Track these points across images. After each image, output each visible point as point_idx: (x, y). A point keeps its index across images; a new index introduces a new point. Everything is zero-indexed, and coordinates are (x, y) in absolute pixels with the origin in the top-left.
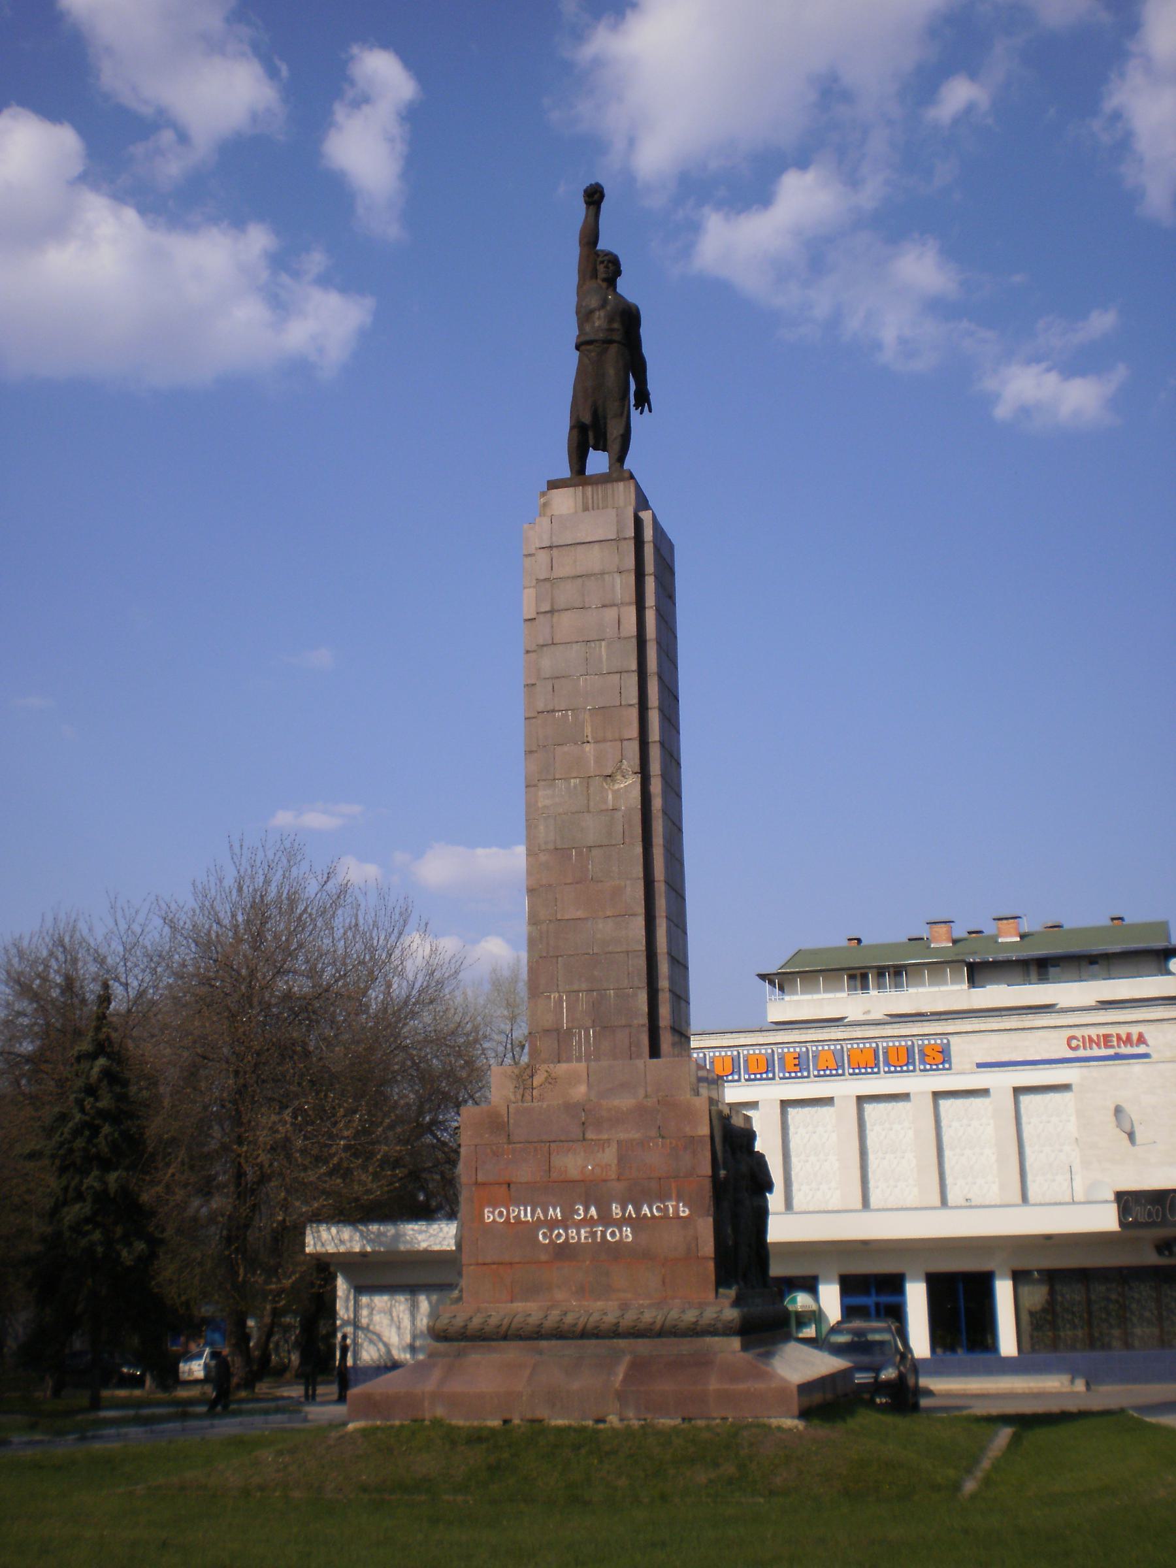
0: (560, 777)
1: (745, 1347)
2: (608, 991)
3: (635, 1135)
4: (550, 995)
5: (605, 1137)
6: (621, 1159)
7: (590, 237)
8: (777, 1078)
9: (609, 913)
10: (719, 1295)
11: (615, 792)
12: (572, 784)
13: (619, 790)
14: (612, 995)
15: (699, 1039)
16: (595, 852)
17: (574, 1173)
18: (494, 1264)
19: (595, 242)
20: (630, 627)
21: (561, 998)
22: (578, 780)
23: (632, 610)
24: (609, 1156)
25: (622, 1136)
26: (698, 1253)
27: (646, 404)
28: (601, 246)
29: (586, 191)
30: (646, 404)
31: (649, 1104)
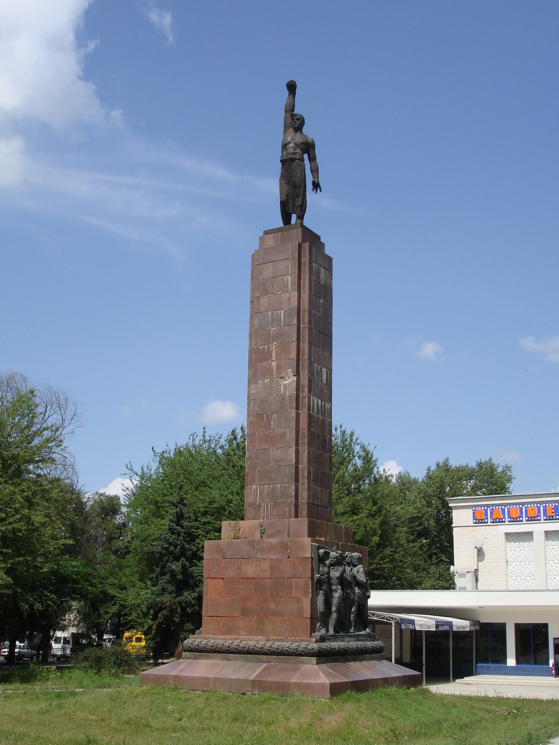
0: (260, 379)
1: (318, 663)
2: (277, 485)
3: (278, 556)
4: (252, 487)
5: (265, 557)
6: (272, 568)
7: (290, 109)
8: (507, 521)
9: (279, 446)
10: (312, 636)
11: (285, 386)
12: (266, 382)
13: (286, 384)
14: (279, 487)
15: (499, 499)
16: (274, 416)
17: (251, 574)
18: (215, 616)
19: (293, 110)
20: (295, 303)
21: (257, 488)
22: (268, 380)
23: (296, 294)
24: (266, 566)
25: (272, 557)
26: (303, 615)
27: (318, 188)
28: (296, 112)
29: (287, 85)
30: (318, 188)
31: (285, 541)
